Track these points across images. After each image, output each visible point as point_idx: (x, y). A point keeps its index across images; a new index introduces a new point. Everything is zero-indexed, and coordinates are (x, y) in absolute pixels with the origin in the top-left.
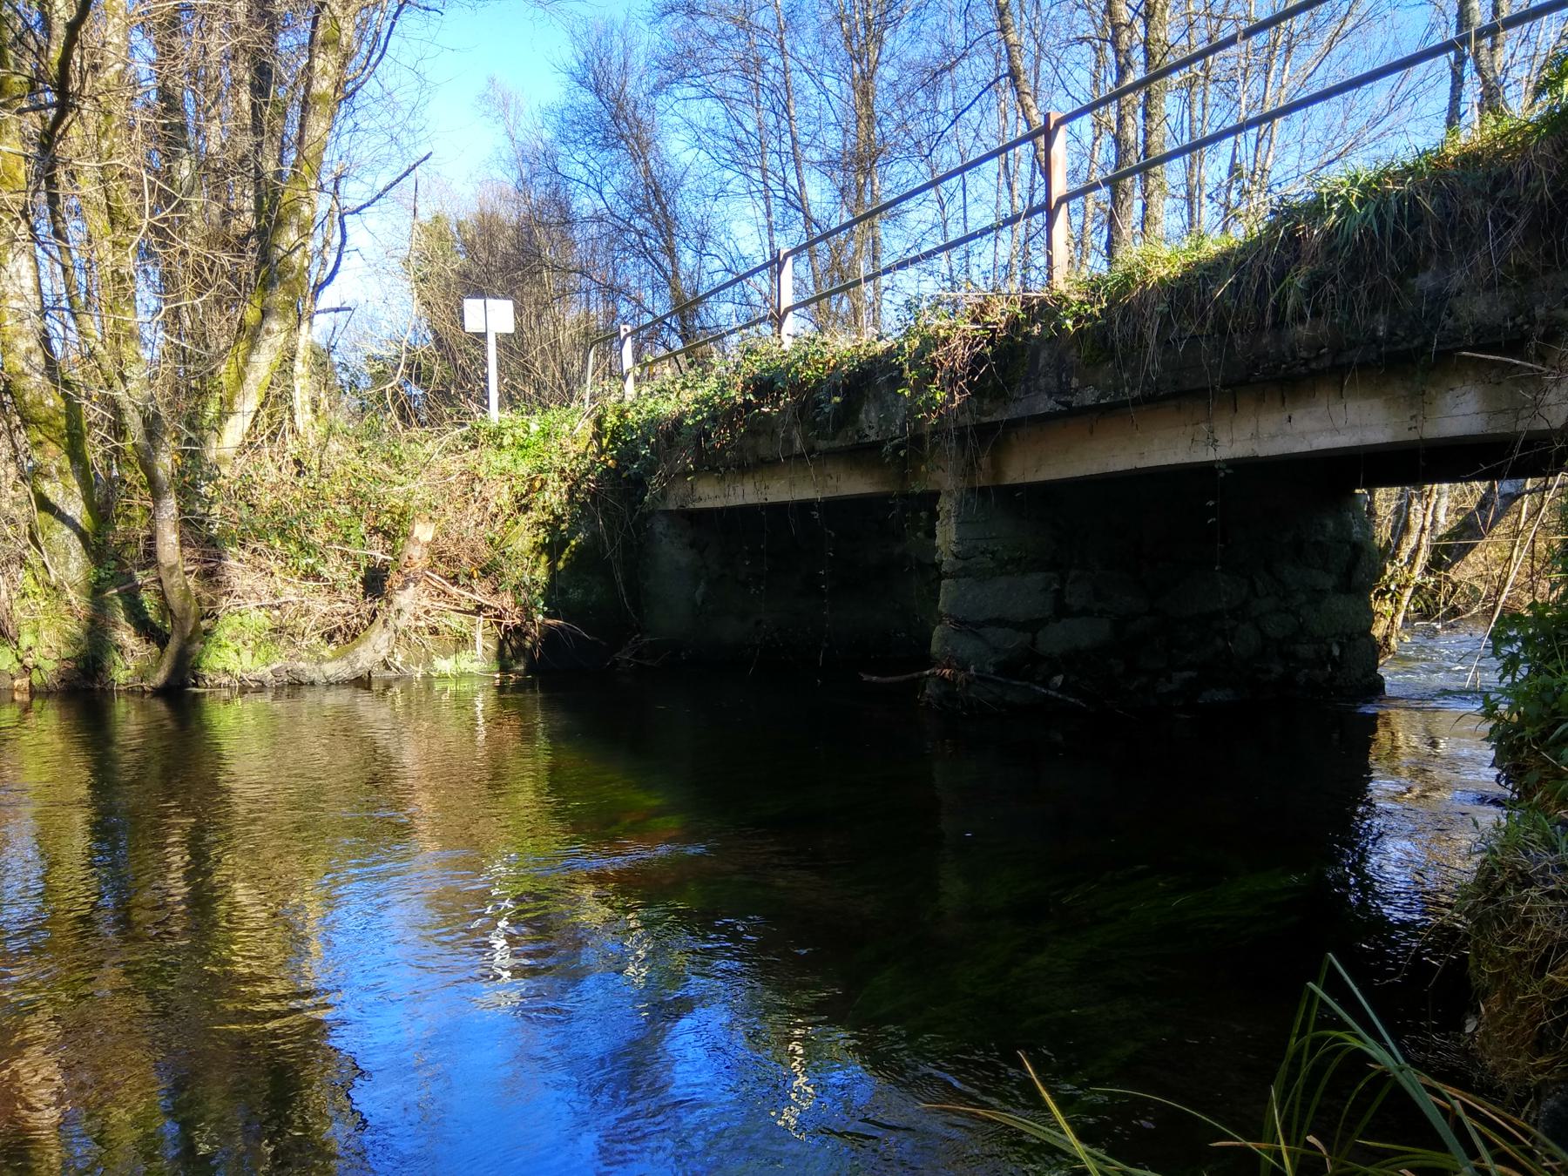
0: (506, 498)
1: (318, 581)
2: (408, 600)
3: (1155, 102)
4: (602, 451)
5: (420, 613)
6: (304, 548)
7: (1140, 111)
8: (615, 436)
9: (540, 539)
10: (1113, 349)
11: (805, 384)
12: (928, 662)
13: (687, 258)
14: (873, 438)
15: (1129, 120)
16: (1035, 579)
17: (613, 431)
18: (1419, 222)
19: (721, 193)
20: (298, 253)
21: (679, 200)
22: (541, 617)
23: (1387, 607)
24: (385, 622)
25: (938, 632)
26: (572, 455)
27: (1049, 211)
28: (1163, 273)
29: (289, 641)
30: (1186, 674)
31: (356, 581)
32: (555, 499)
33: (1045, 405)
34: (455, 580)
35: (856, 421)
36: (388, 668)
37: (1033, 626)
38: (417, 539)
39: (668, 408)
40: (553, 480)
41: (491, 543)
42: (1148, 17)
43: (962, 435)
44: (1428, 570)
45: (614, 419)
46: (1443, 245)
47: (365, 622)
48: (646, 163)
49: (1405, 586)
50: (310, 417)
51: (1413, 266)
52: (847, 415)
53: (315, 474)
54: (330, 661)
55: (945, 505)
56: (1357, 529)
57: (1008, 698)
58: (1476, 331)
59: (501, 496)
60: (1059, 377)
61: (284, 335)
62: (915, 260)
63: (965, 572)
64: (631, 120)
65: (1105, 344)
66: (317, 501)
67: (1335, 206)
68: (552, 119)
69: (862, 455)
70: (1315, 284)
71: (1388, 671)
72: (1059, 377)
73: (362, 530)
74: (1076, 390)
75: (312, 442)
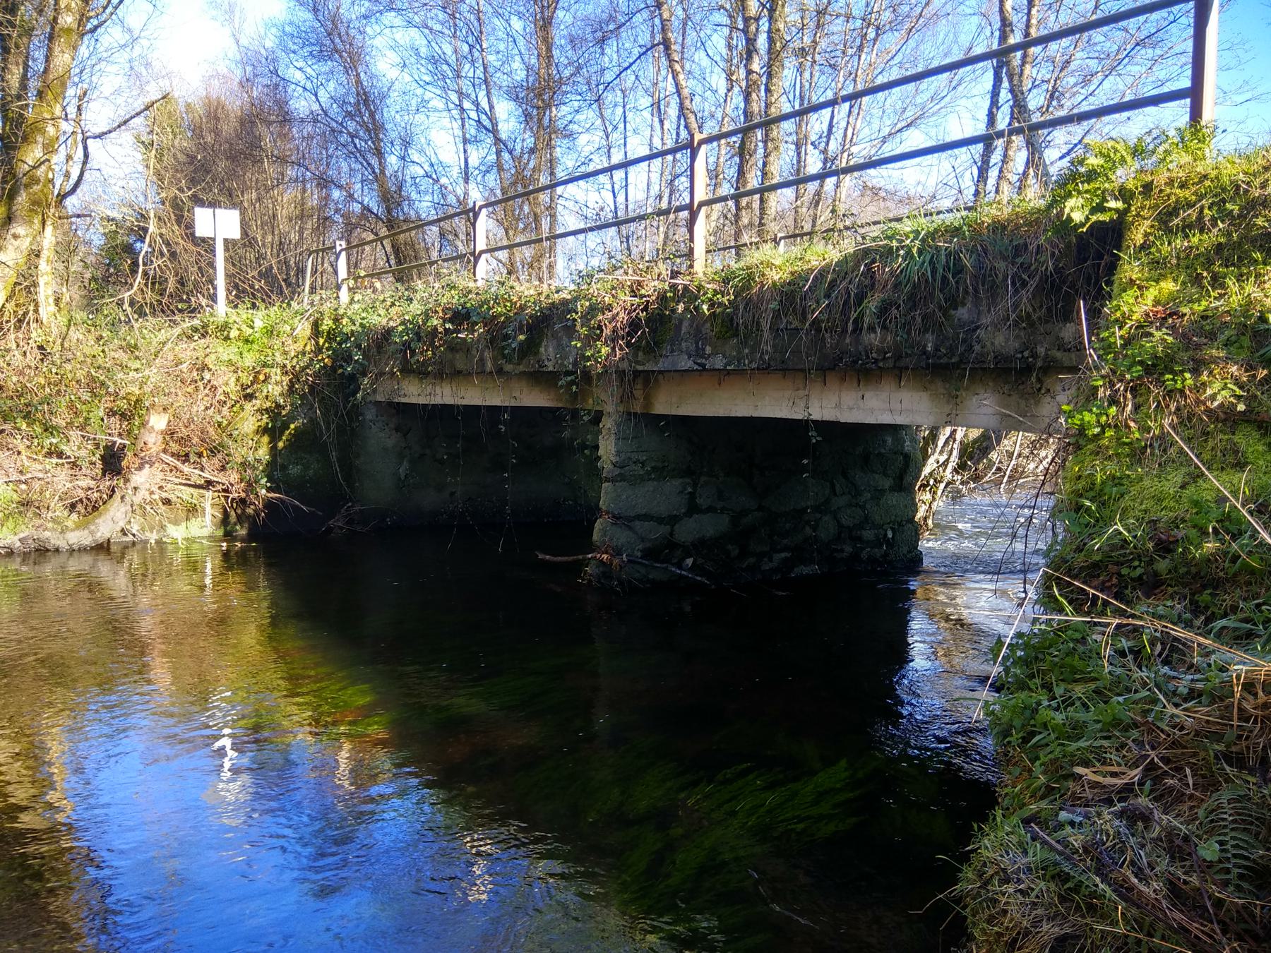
0: (232, 387)
1: (61, 458)
2: (144, 480)
3: (774, 80)
4: (319, 350)
5: (155, 489)
6: (48, 429)
7: (763, 88)
8: (331, 336)
9: (263, 423)
10: (737, 329)
11: (494, 317)
12: (591, 547)
13: (392, 161)
14: (551, 369)
15: (754, 95)
16: (673, 485)
17: (329, 332)
18: (960, 272)
19: (423, 104)
20: (43, 168)
21: (385, 110)
22: (264, 491)
23: (927, 496)
24: (123, 497)
25: (598, 525)
26: (293, 354)
27: (692, 148)
28: (776, 278)
29: (35, 513)
30: (783, 555)
31: (96, 458)
32: (278, 390)
33: (686, 363)
34: (185, 458)
35: (537, 353)
36: (125, 534)
37: (673, 520)
38: (152, 427)
39: (379, 320)
40: (276, 375)
41: (219, 426)
42: (772, 11)
43: (620, 374)
44: (955, 471)
45: (330, 322)
46: (976, 290)
47: (105, 496)
48: (358, 75)
49: (941, 482)
50: (53, 308)
51: (954, 302)
52: (530, 348)
53: (56, 358)
54: (72, 530)
55: (607, 423)
56: (908, 443)
57: (651, 577)
58: (996, 357)
59: (228, 383)
60: (697, 344)
61: (29, 239)
62: (585, 176)
63: (622, 477)
64: (345, 38)
65: (732, 325)
66: (59, 383)
67: (902, 252)
68: (274, 30)
69: (541, 378)
70: (884, 309)
71: (927, 544)
72: (697, 344)
73: (101, 414)
74: (709, 355)
75: (55, 331)
